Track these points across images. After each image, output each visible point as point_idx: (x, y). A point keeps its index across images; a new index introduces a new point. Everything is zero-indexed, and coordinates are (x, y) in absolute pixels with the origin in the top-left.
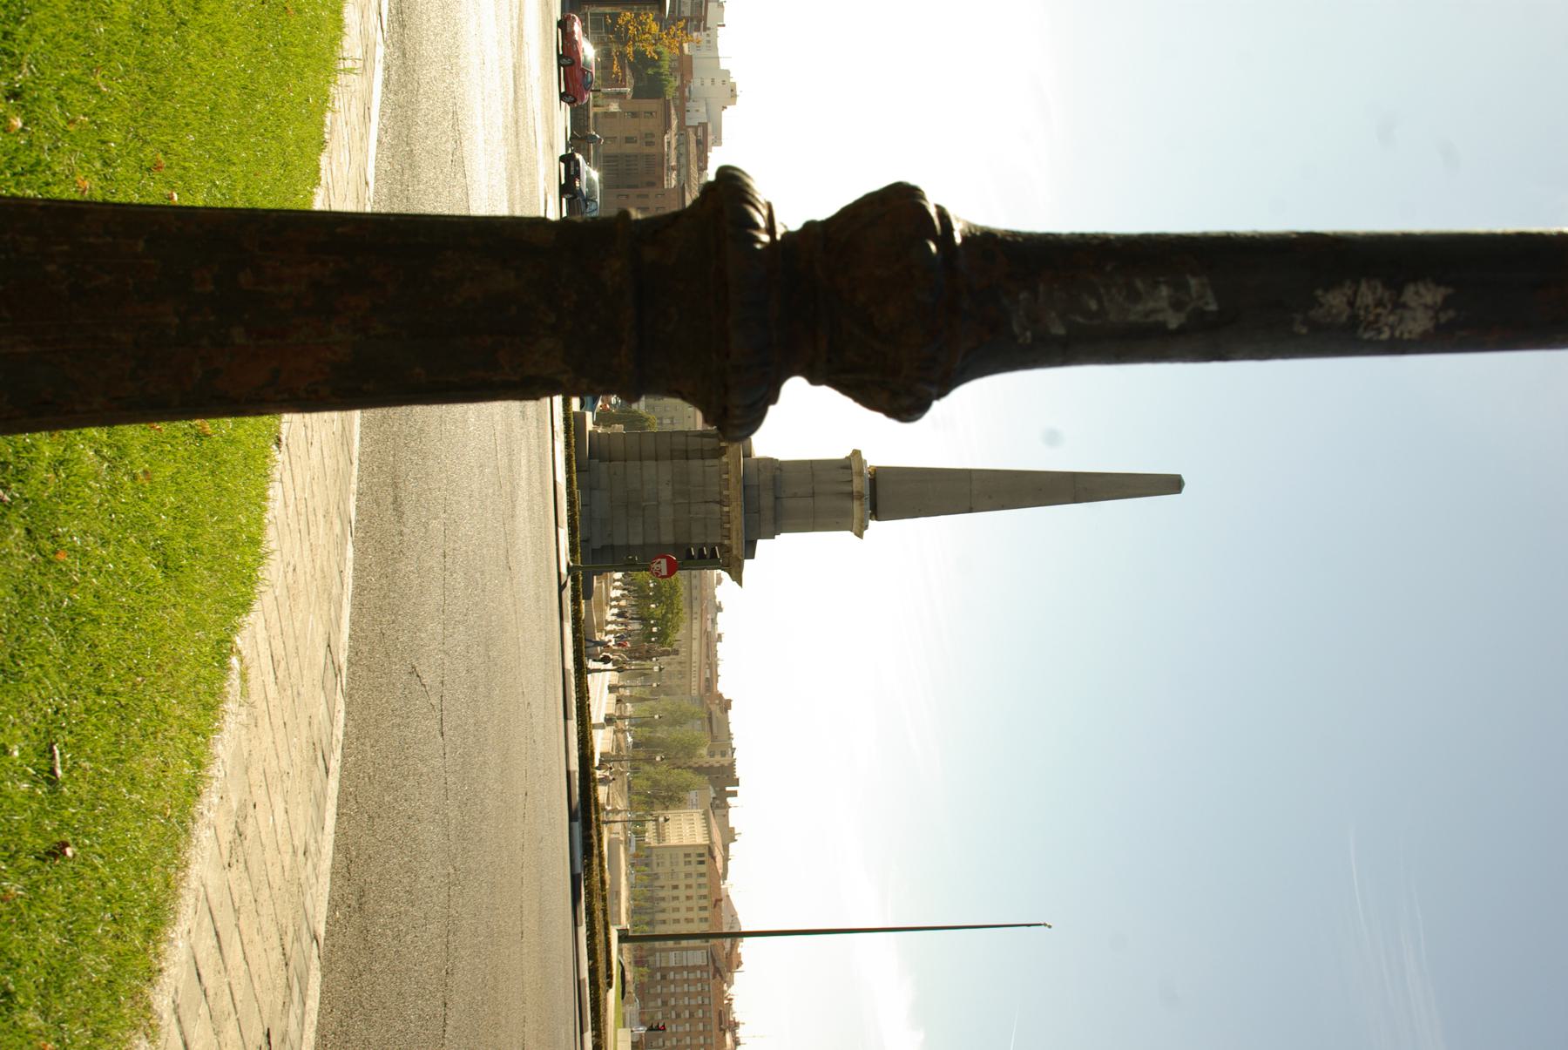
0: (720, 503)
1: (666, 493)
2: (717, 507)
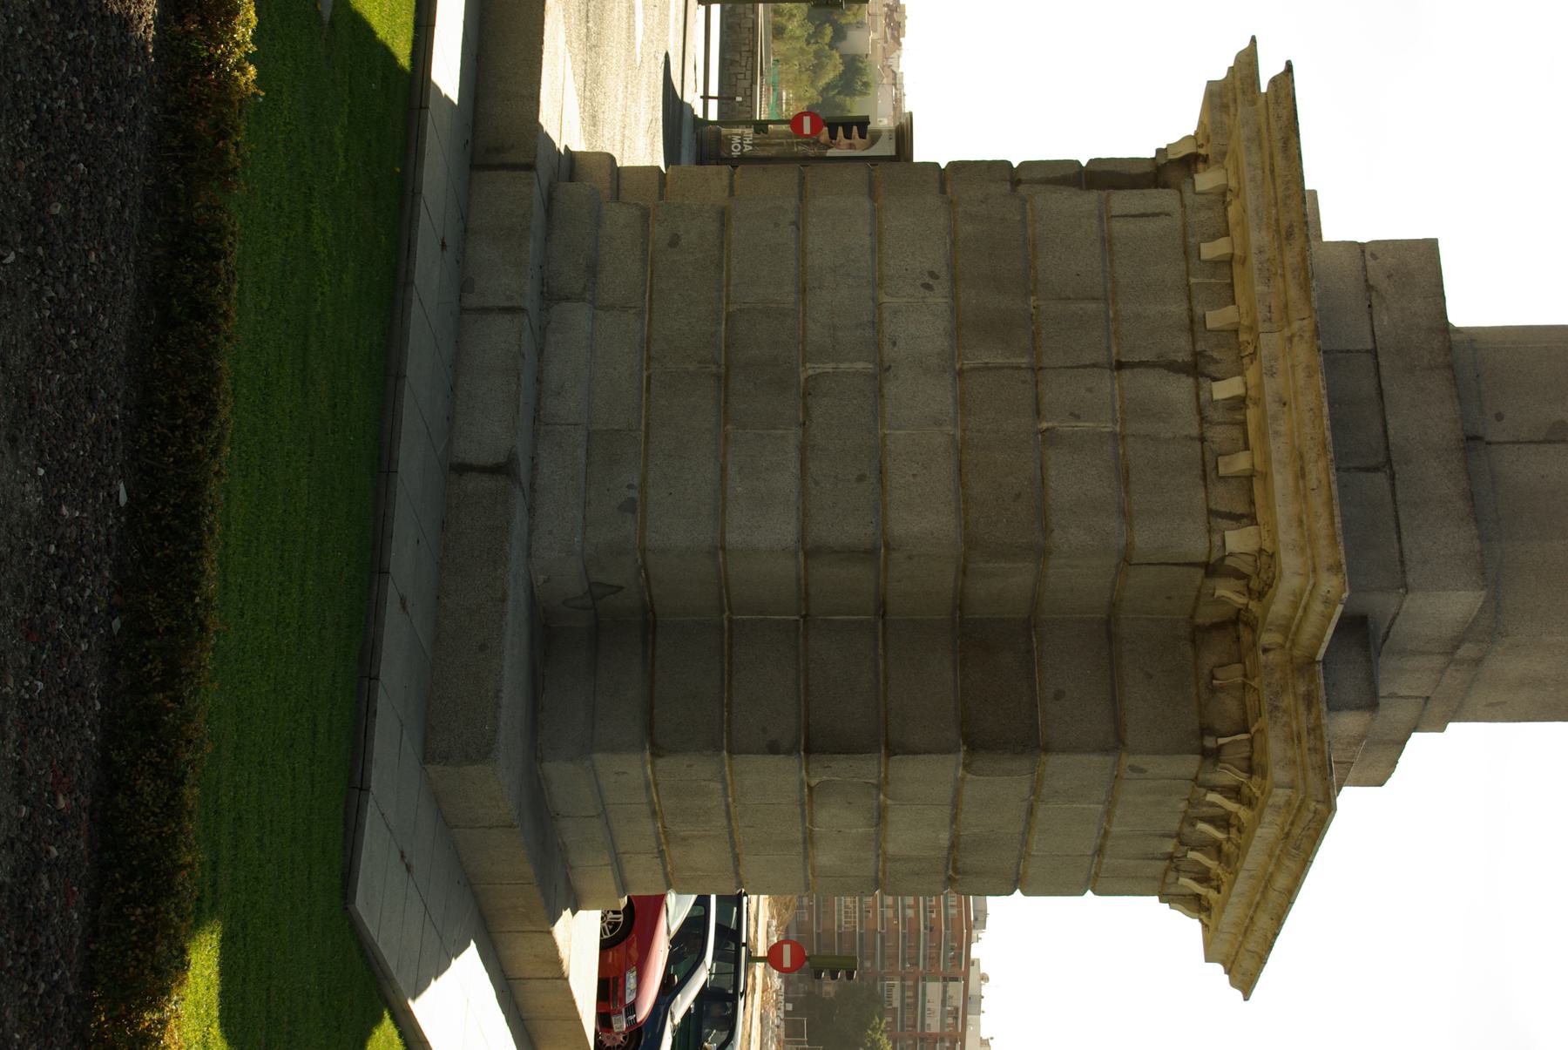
0: (1196, 368)
1: (920, 327)
2: (1179, 389)
